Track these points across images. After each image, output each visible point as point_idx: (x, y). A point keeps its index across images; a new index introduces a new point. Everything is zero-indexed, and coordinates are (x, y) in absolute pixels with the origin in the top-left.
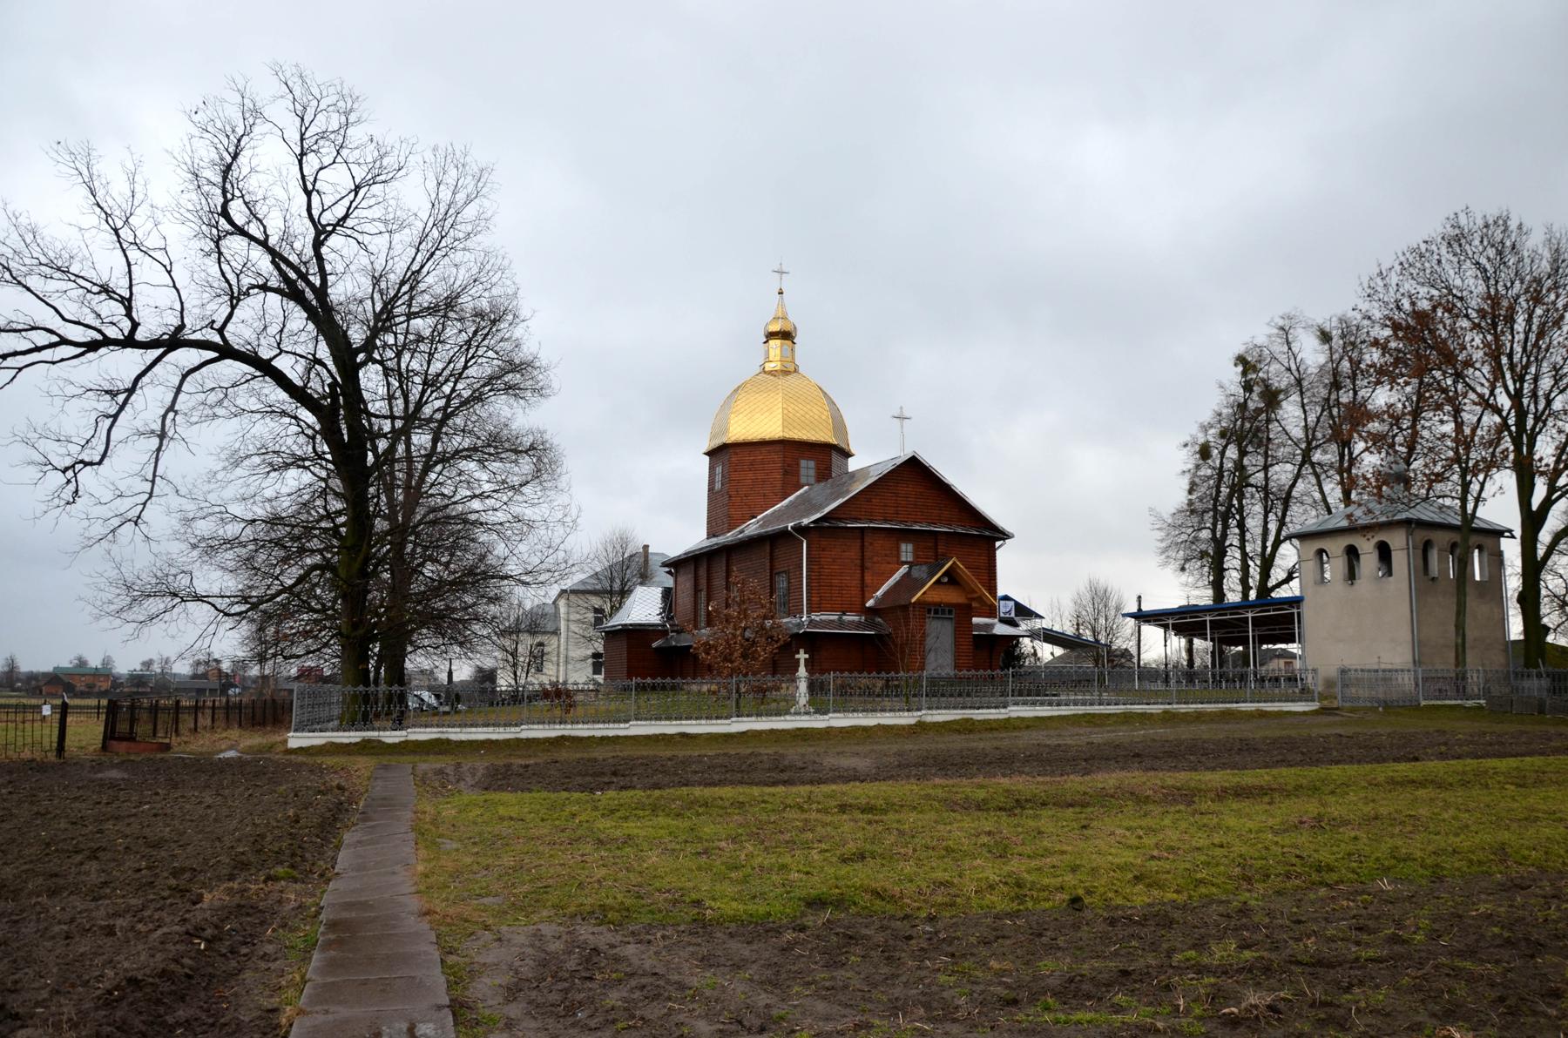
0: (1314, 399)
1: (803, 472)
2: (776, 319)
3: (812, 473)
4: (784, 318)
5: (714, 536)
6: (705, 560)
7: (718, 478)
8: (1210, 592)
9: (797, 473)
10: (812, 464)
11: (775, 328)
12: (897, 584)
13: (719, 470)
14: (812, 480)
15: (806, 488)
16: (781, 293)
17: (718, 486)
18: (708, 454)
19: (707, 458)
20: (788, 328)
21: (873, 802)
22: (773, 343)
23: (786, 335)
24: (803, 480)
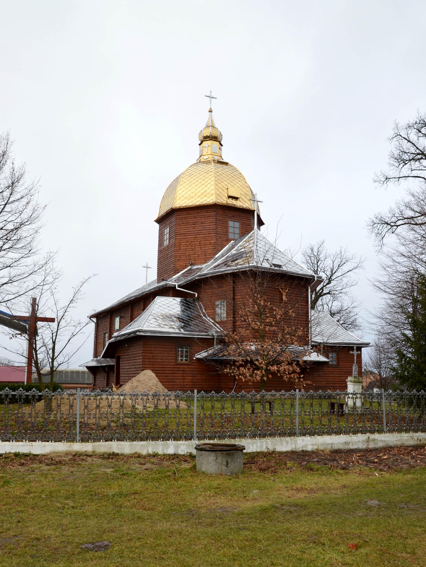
0: (47, 508)
1: (231, 230)
2: (208, 127)
3: (237, 231)
4: (213, 127)
5: (163, 280)
6: (130, 307)
7: (167, 237)
8: (25, 360)
9: (227, 233)
10: (237, 224)
11: (207, 133)
12: (190, 293)
13: (167, 231)
14: (237, 236)
15: (232, 242)
16: (211, 111)
17: (166, 243)
18: (160, 221)
19: (157, 226)
20: (215, 134)
21: (262, 474)
22: (205, 143)
23: (215, 138)
24: (231, 236)
